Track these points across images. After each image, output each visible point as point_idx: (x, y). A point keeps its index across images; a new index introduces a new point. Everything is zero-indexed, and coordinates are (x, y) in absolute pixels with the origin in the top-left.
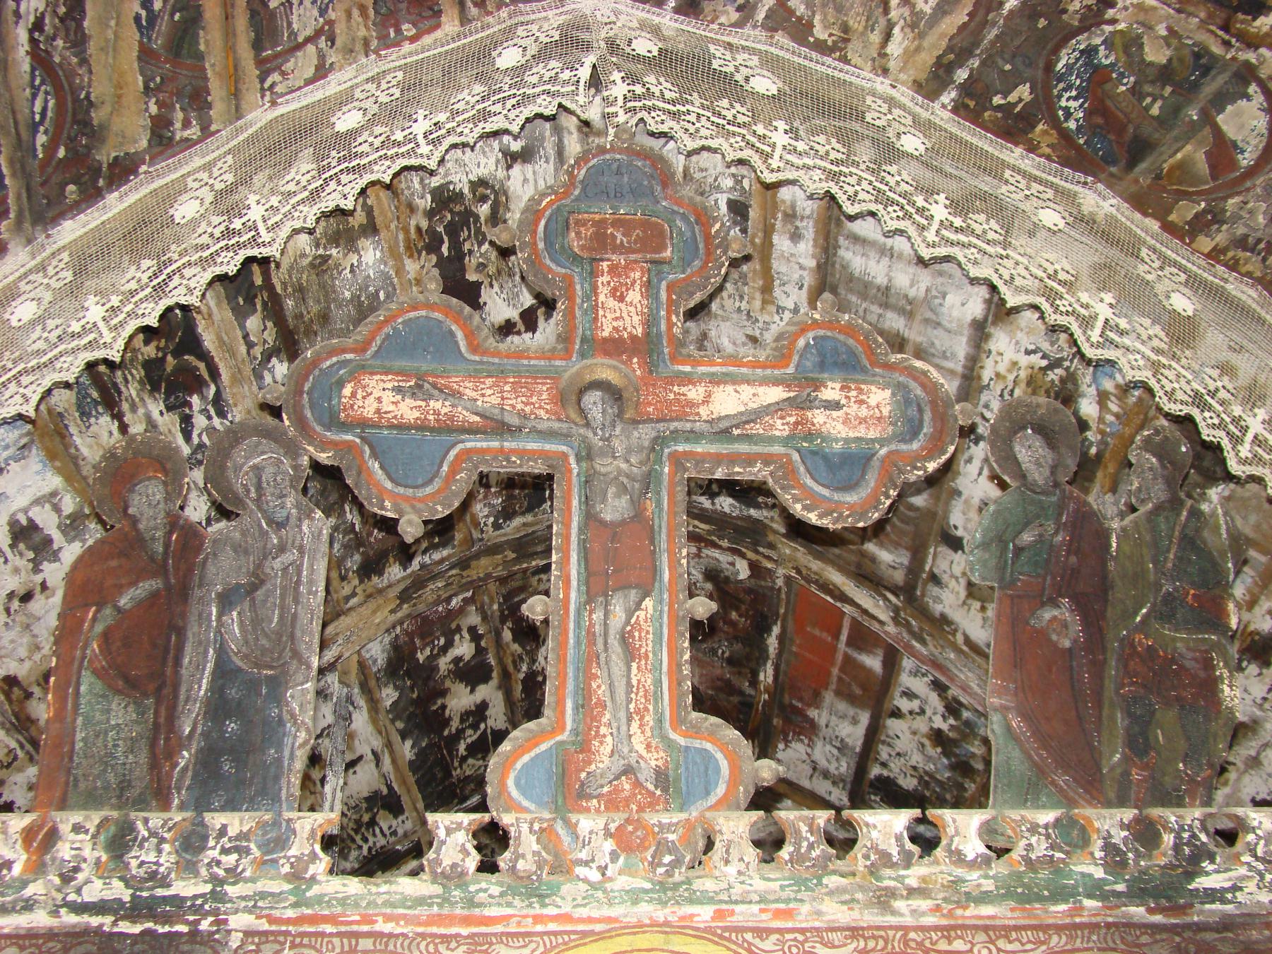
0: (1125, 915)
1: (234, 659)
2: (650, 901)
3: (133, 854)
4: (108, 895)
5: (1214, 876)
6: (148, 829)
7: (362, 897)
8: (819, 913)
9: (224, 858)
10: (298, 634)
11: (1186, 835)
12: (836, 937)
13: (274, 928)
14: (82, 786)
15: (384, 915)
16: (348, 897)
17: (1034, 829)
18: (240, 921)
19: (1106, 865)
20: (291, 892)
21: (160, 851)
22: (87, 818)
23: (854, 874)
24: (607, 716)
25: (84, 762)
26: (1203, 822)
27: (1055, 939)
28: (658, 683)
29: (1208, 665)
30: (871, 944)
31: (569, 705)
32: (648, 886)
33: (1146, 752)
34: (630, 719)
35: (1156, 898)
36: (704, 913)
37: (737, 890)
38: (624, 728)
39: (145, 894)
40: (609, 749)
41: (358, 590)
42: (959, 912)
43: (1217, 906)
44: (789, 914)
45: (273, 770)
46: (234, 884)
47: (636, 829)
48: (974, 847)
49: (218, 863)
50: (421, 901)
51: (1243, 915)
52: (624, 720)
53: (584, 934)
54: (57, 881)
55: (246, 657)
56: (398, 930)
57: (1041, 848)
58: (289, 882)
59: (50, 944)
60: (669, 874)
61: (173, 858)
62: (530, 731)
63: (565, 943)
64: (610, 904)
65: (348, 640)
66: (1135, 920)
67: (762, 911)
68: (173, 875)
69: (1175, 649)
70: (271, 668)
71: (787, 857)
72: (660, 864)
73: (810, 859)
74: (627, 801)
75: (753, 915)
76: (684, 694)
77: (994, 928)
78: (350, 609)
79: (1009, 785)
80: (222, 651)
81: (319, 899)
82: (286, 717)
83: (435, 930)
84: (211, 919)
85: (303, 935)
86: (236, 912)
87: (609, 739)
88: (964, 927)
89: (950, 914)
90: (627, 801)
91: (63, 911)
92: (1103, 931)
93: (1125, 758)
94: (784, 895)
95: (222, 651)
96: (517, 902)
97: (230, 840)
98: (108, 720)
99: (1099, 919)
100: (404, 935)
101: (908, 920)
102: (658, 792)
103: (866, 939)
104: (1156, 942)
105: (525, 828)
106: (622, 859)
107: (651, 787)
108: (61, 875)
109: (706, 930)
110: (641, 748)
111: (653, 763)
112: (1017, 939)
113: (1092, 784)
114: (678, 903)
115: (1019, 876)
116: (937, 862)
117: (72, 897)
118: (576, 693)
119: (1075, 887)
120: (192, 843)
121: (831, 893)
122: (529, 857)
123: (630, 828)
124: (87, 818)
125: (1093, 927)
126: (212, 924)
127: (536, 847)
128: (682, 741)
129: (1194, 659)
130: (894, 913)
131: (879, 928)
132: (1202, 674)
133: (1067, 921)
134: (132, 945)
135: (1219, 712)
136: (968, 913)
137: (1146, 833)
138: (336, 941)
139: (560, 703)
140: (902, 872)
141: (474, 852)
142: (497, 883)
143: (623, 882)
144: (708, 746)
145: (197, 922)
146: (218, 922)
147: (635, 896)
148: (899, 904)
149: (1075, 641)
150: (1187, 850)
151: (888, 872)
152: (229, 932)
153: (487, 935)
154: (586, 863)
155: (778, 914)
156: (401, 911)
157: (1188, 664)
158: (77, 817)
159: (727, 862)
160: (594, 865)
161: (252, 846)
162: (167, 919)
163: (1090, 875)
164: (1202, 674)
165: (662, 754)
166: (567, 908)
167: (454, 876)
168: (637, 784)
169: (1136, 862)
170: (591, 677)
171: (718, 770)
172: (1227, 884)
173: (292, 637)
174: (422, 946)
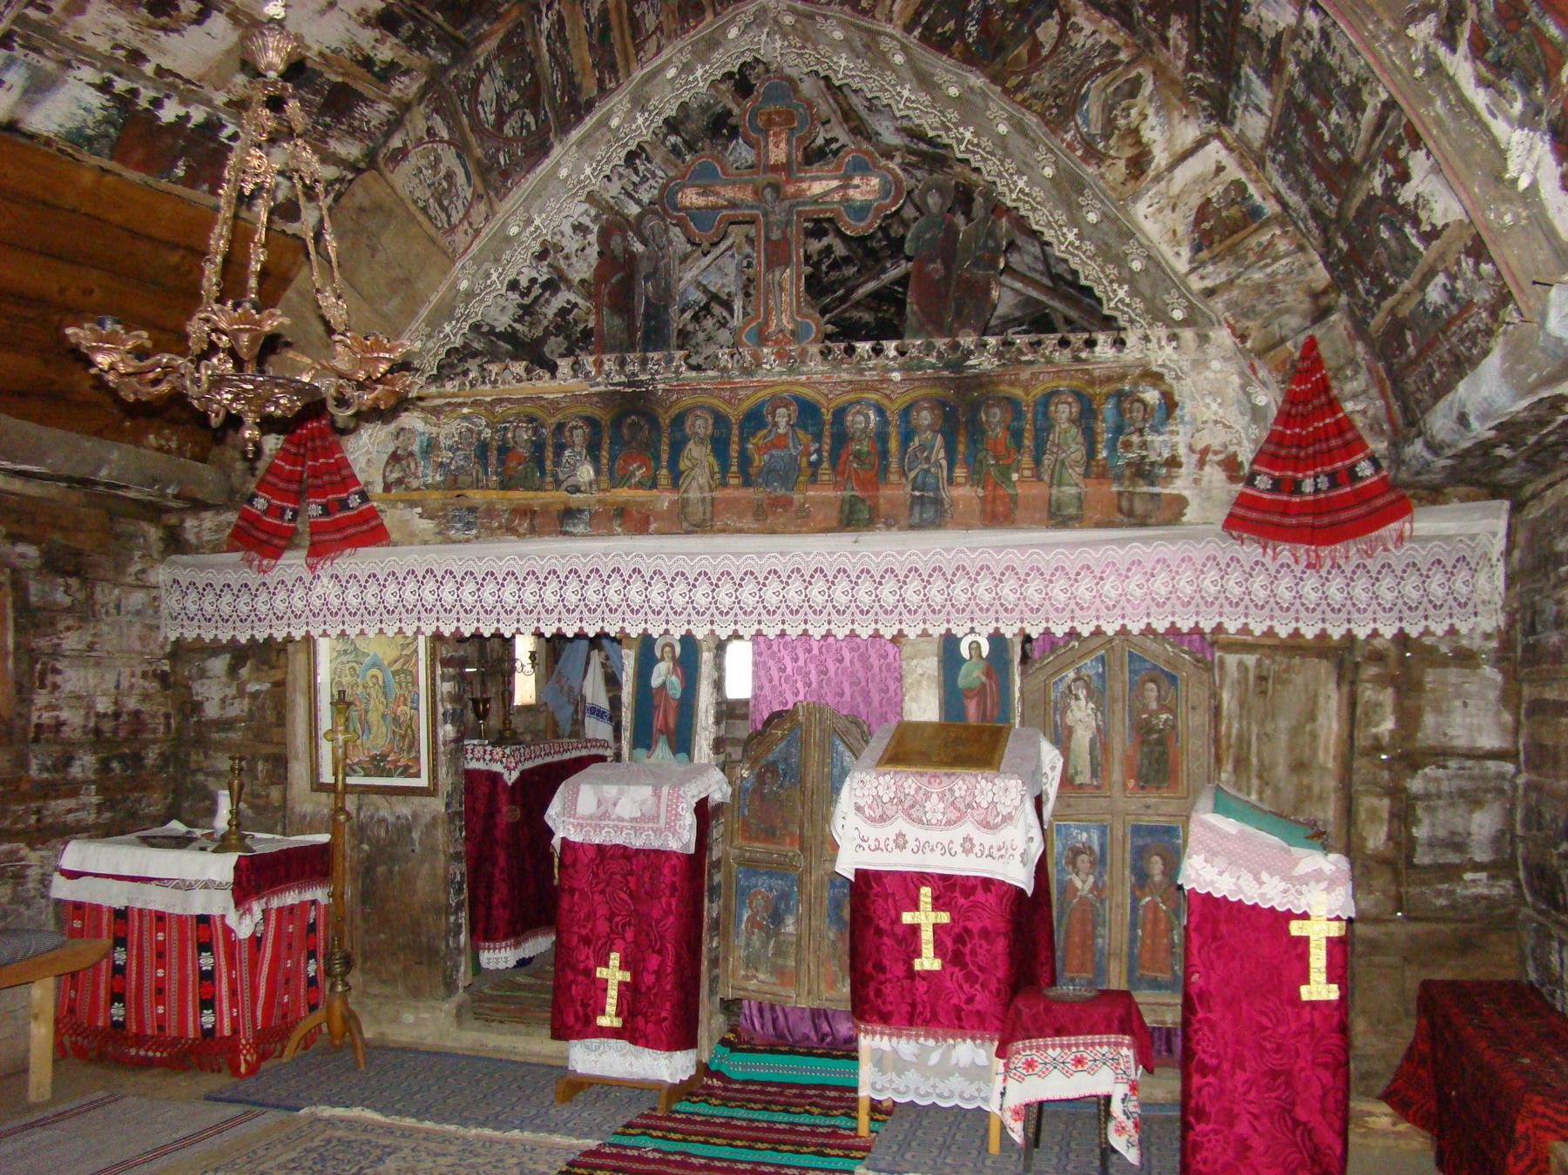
18: (660, 386)
29: (989, 283)
36: (803, 378)
48: (892, 353)
120: (644, 362)
147: (781, 373)
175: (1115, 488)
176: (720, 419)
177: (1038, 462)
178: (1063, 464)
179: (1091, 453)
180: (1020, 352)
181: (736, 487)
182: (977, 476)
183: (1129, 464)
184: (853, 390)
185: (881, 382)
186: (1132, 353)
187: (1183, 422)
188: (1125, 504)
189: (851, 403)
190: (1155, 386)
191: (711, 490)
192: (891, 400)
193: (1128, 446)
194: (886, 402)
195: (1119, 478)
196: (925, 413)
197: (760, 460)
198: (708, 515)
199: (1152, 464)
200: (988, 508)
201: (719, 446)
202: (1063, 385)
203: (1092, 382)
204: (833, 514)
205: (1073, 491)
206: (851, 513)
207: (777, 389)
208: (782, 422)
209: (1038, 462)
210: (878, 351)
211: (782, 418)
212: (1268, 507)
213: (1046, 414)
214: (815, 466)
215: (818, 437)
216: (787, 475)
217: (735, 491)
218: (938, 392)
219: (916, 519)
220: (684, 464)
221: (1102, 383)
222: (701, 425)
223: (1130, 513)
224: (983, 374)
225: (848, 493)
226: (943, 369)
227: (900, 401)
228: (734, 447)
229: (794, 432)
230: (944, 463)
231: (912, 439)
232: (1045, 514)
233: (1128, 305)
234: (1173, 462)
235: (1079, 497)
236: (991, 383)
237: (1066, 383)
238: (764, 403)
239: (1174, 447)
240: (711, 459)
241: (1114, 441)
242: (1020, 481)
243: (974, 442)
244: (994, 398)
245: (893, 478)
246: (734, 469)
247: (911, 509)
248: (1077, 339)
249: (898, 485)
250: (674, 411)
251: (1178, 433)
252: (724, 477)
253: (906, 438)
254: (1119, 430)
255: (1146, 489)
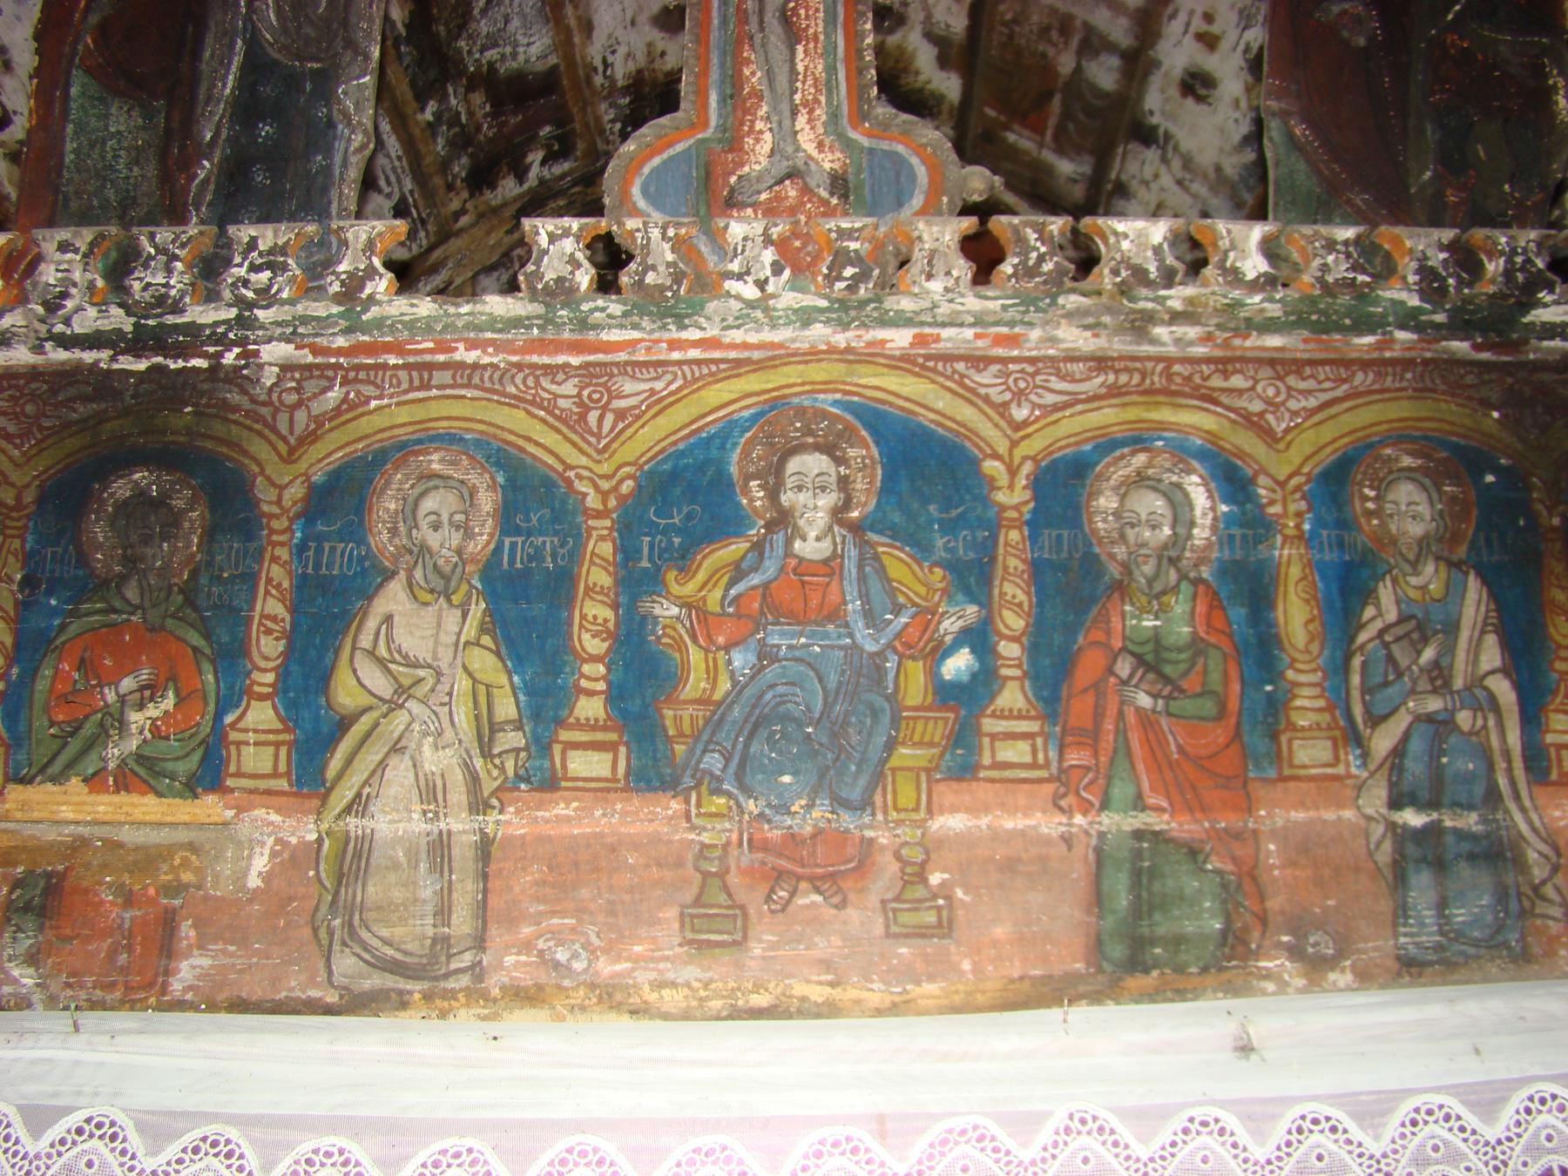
0: (1445, 351)
1: (270, 51)
2: (827, 322)
3: (136, 275)
4: (105, 325)
5: (1553, 309)
6: (156, 247)
7: (436, 319)
8: (1053, 340)
9: (253, 277)
10: (353, 20)
11: (1519, 259)
12: (1078, 368)
13: (319, 360)
14: (74, 205)
15: (466, 340)
16: (418, 320)
17: (1331, 245)
18: (274, 352)
19: (1423, 294)
20: (341, 315)
21: (169, 271)
22: (76, 234)
23: (1099, 293)
24: (764, 110)
25: (76, 177)
26: (1539, 244)
27: (1359, 377)
28: (831, 70)
29: (1540, 74)
30: (1123, 378)
31: (713, 99)
32: (824, 303)
34: (794, 113)
35: (1484, 333)
36: (900, 339)
37: (944, 309)
38: (787, 123)
39: (151, 322)
40: (767, 148)
41: (469, 206)
42: (1237, 342)
44: (1014, 341)
45: (320, 179)
46: (267, 307)
47: (804, 245)
48: (1254, 265)
49: (246, 283)
50: (516, 323)
52: (787, 114)
53: (738, 363)
54: (40, 310)
55: (285, 47)
56: (486, 360)
57: (1339, 269)
58: (339, 304)
59: (34, 386)
60: (852, 289)
61: (187, 278)
62: (664, 127)
63: (711, 374)
64: (773, 327)
65: (459, 264)
66: (1459, 356)
67: (977, 336)
68: (187, 300)
70: (317, 60)
71: (1010, 270)
72: (839, 278)
73: (1040, 274)
74: (793, 211)
75: (966, 341)
76: (866, 87)
77: (1283, 362)
78: (461, 230)
79: (1293, 202)
80: (253, 43)
81: (379, 323)
82: (336, 116)
83: (535, 359)
84: (237, 350)
85: (358, 368)
86: (269, 341)
87: (768, 136)
88: (1242, 359)
89: (1226, 344)
90: (793, 211)
91: (48, 345)
92: (1419, 369)
94: (1008, 316)
95: (253, 43)
96: (646, 323)
97: (261, 255)
98: (106, 128)
99: (1413, 354)
100: (494, 366)
101: (1171, 350)
102: (834, 201)
103: (1117, 372)
104: (1484, 383)
105: (655, 233)
106: (787, 273)
107: (824, 194)
108: (45, 304)
109: (902, 358)
110: (810, 148)
111: (827, 166)
112: (1312, 376)
113: (1396, 204)
114: (863, 325)
115: (1313, 301)
116: (1205, 284)
117: (59, 328)
118: (722, 82)
119: (1384, 316)
120: (210, 268)
121: (1069, 315)
122: (661, 268)
123: (797, 244)
124: (76, 234)
125: (1407, 364)
126: (238, 357)
127: (670, 257)
128: (865, 142)
130: (1154, 341)
133: (1375, 355)
134: (136, 385)
136: (1248, 343)
137: (1466, 260)
138: (403, 374)
139: (702, 94)
140: (1163, 293)
141: (586, 264)
142: (618, 302)
143: (789, 299)
144: (900, 148)
145: (220, 355)
146: (245, 355)
147: (805, 317)
148: (1160, 331)
149: (1371, 39)
150: (1520, 277)
151: (1144, 292)
152: (261, 366)
153: (605, 364)
154: (740, 277)
155: (999, 340)
156: (489, 335)
158: (63, 234)
159: (929, 277)
160: (749, 279)
161: (290, 261)
162: (182, 352)
163: (1402, 303)
165: (838, 155)
166: (713, 332)
167: (562, 291)
168: (806, 190)
169: (1458, 288)
170: (740, 62)
171: (913, 177)
173: (345, 23)
174: (519, 379)
176: (530, 494)
181: (601, 790)
184: (1114, 391)
189: (1109, 445)
191: (479, 805)
192: (1267, 434)
197: (706, 674)
198: (462, 923)
201: (523, 605)
204: (1060, 923)
206: (1141, 908)
207: (790, 375)
208: (814, 512)
211: (813, 495)
212: (43, 440)
214: (963, 701)
215: (973, 577)
216: (840, 738)
217: (596, 803)
218: (1449, 413)
219: (1422, 933)
220: (356, 682)
222: (446, 517)
225: (1117, 822)
227: (1305, 443)
228: (592, 620)
229: (870, 558)
230: (1503, 688)
231: (1368, 595)
238: (728, 430)
240: (485, 663)
245: (1310, 753)
246: (591, 708)
247: (1400, 878)
249: (1329, 785)
250: (322, 459)
252: (541, 746)
253: (1348, 587)
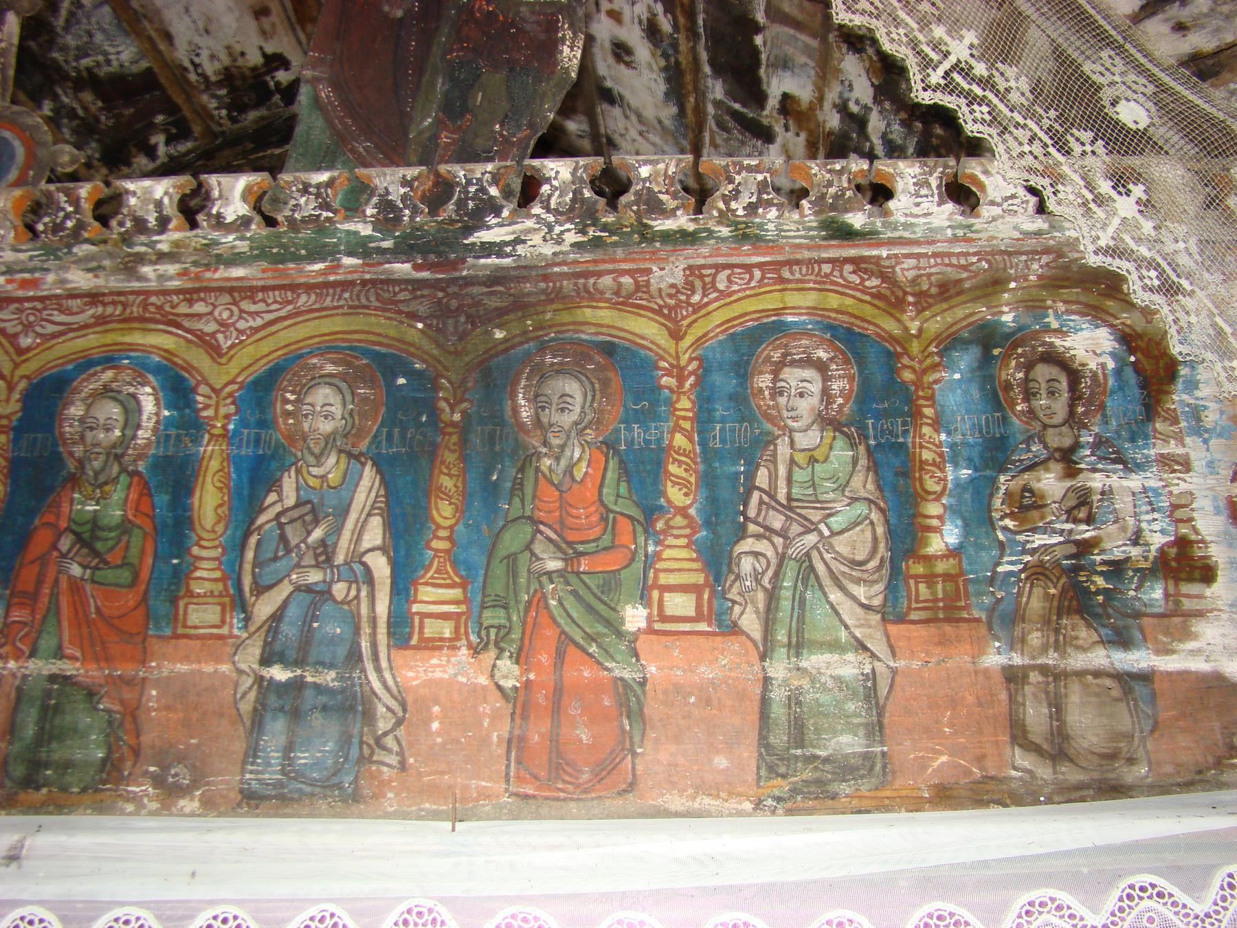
0: (385, 272)
5: (496, 229)
8: (64, 281)
11: (472, 189)
29: (552, 27)
33: (462, 115)
42: (208, 275)
43: (493, 260)
44: (34, 284)
51: (518, 267)
69: (518, 13)
88: (207, 290)
93: (438, 123)
94: (31, 264)
99: (355, 276)
101: (153, 285)
104: (415, 298)
121: (79, 261)
125: (346, 285)
129: (538, 23)
131: (120, 293)
132: (542, 37)
135: (553, 72)
148: (147, 270)
150: (471, 204)
157: (528, 27)
163: (356, 233)
164: (542, 37)
169: (412, 218)
171: (12, 156)
172: (508, 238)
175: (995, 658)
177: (717, 562)
178: (807, 572)
179: (905, 536)
180: (655, 207)
182: (498, 615)
183: (1037, 572)
185: (190, 295)
186: (1004, 218)
187: (1198, 429)
188: (1036, 715)
189: (87, 364)
190: (1096, 314)
192: (214, 350)
193: (1027, 506)
194: (200, 359)
195: (1008, 621)
196: (323, 396)
199: (1117, 568)
200: (537, 734)
202: (799, 304)
203: (893, 298)
205: (849, 667)
209: (717, 562)
210: (192, 208)
213: (741, 399)
221: (924, 301)
223: (1058, 748)
224: (525, 271)
226: (399, 252)
227: (246, 355)
230: (380, 565)
231: (274, 484)
232: (748, 752)
233: (980, 82)
234: (1184, 564)
235: (869, 689)
236: (555, 297)
237: (809, 299)
239: (1179, 510)
241: (982, 489)
242: (665, 643)
243: (491, 491)
244: (560, 347)
245: (202, 616)
248: (832, 176)
249: (214, 643)
251: (1186, 465)
254: (995, 453)
255: (1100, 658)
